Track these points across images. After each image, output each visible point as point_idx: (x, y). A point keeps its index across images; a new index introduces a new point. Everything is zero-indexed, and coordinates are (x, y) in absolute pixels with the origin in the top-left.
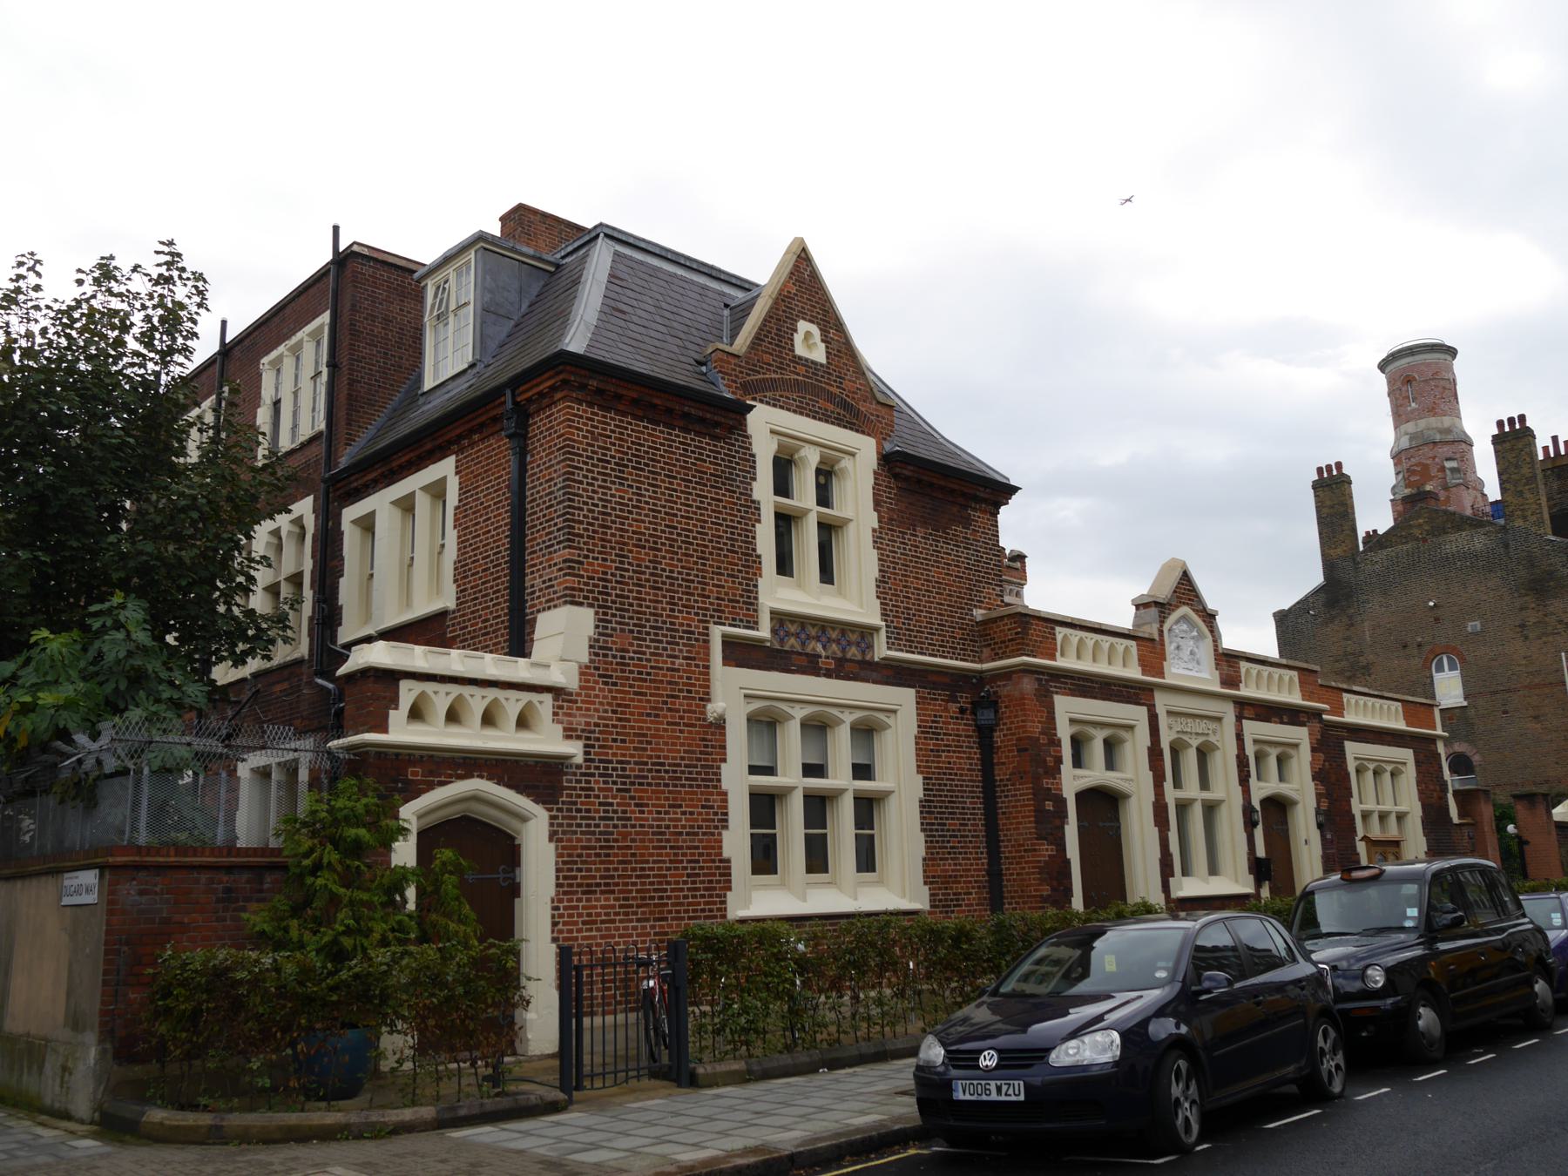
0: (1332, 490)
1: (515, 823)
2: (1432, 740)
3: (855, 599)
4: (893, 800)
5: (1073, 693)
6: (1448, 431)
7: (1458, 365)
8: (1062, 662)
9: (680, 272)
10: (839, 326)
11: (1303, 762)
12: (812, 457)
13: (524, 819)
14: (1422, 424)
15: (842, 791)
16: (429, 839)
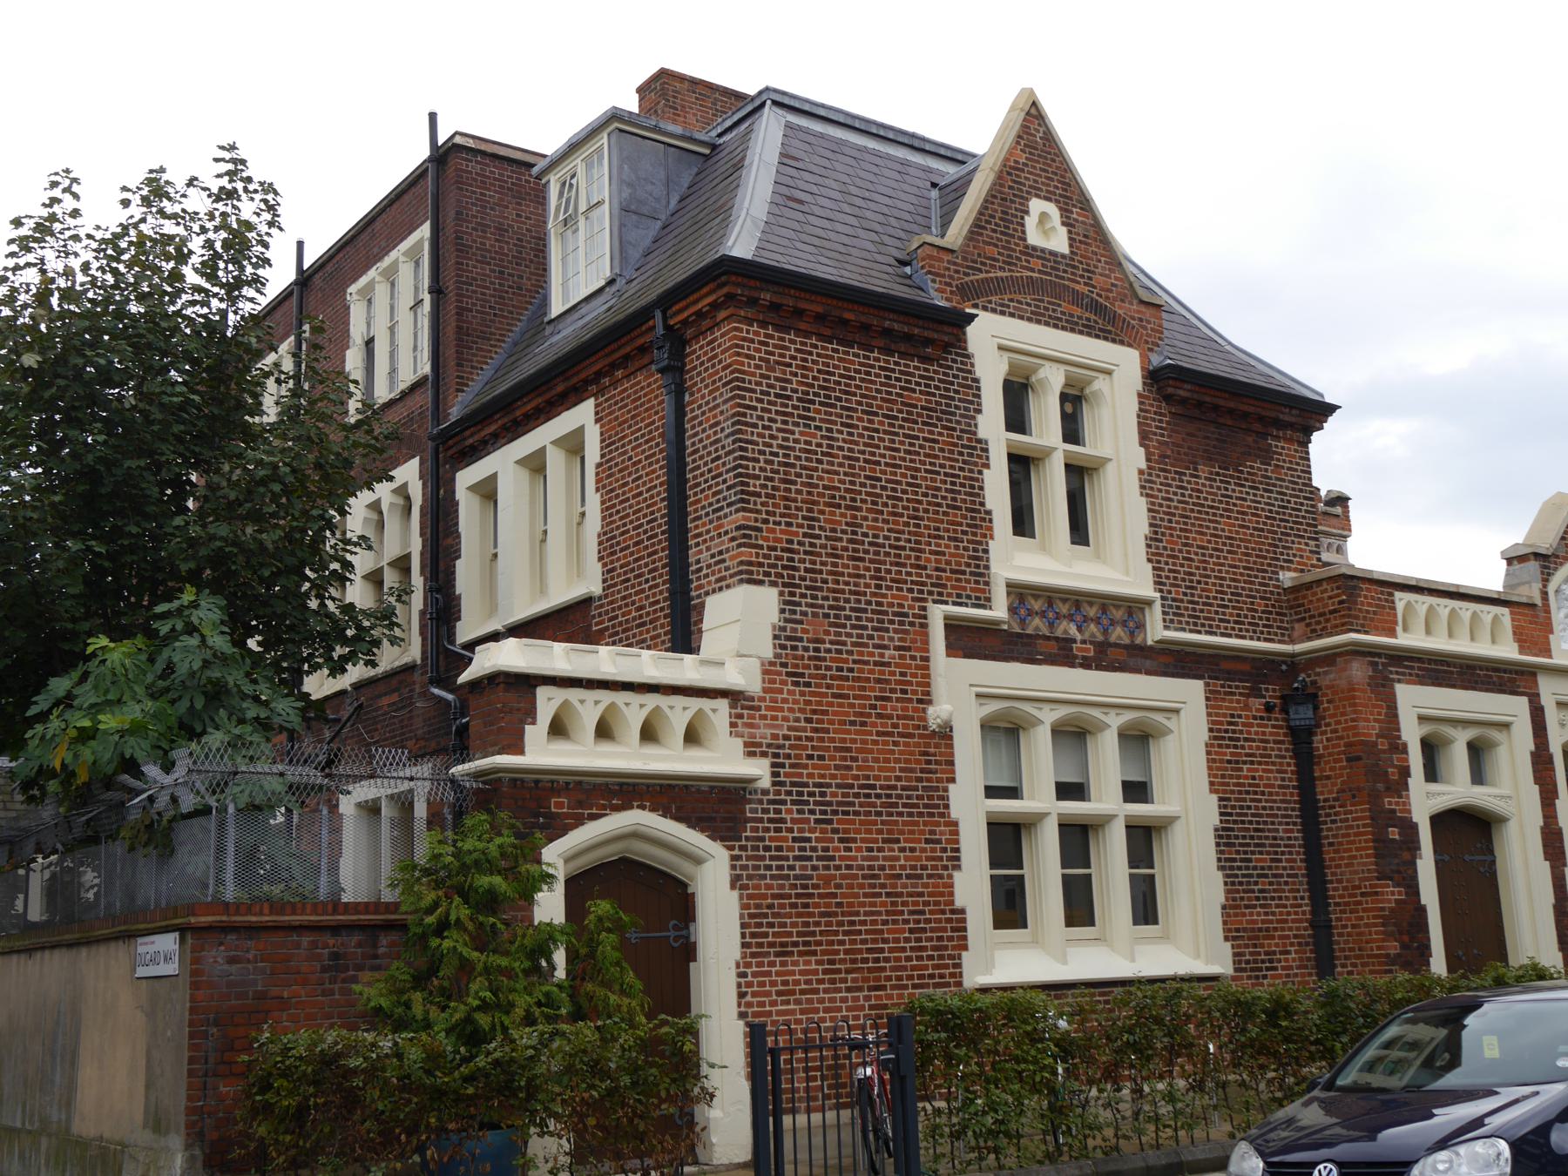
9: (871, 144)
12: (1053, 380)
13: (698, 861)
16: (580, 887)
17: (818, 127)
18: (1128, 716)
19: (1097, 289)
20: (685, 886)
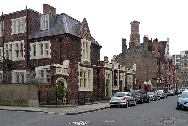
0: (124, 41)
1: (63, 81)
2: (135, 75)
3: (89, 60)
4: (90, 80)
5: (107, 70)
6: (137, 34)
7: (140, 25)
8: (106, 67)
9: (69, 18)
10: (89, 29)
11: (124, 77)
12: (86, 43)
13: (64, 81)
14: (134, 32)
15: (87, 79)
16: (60, 81)
17: (74, 21)
18: (40, 70)
19: (90, 38)
20: (63, 83)
